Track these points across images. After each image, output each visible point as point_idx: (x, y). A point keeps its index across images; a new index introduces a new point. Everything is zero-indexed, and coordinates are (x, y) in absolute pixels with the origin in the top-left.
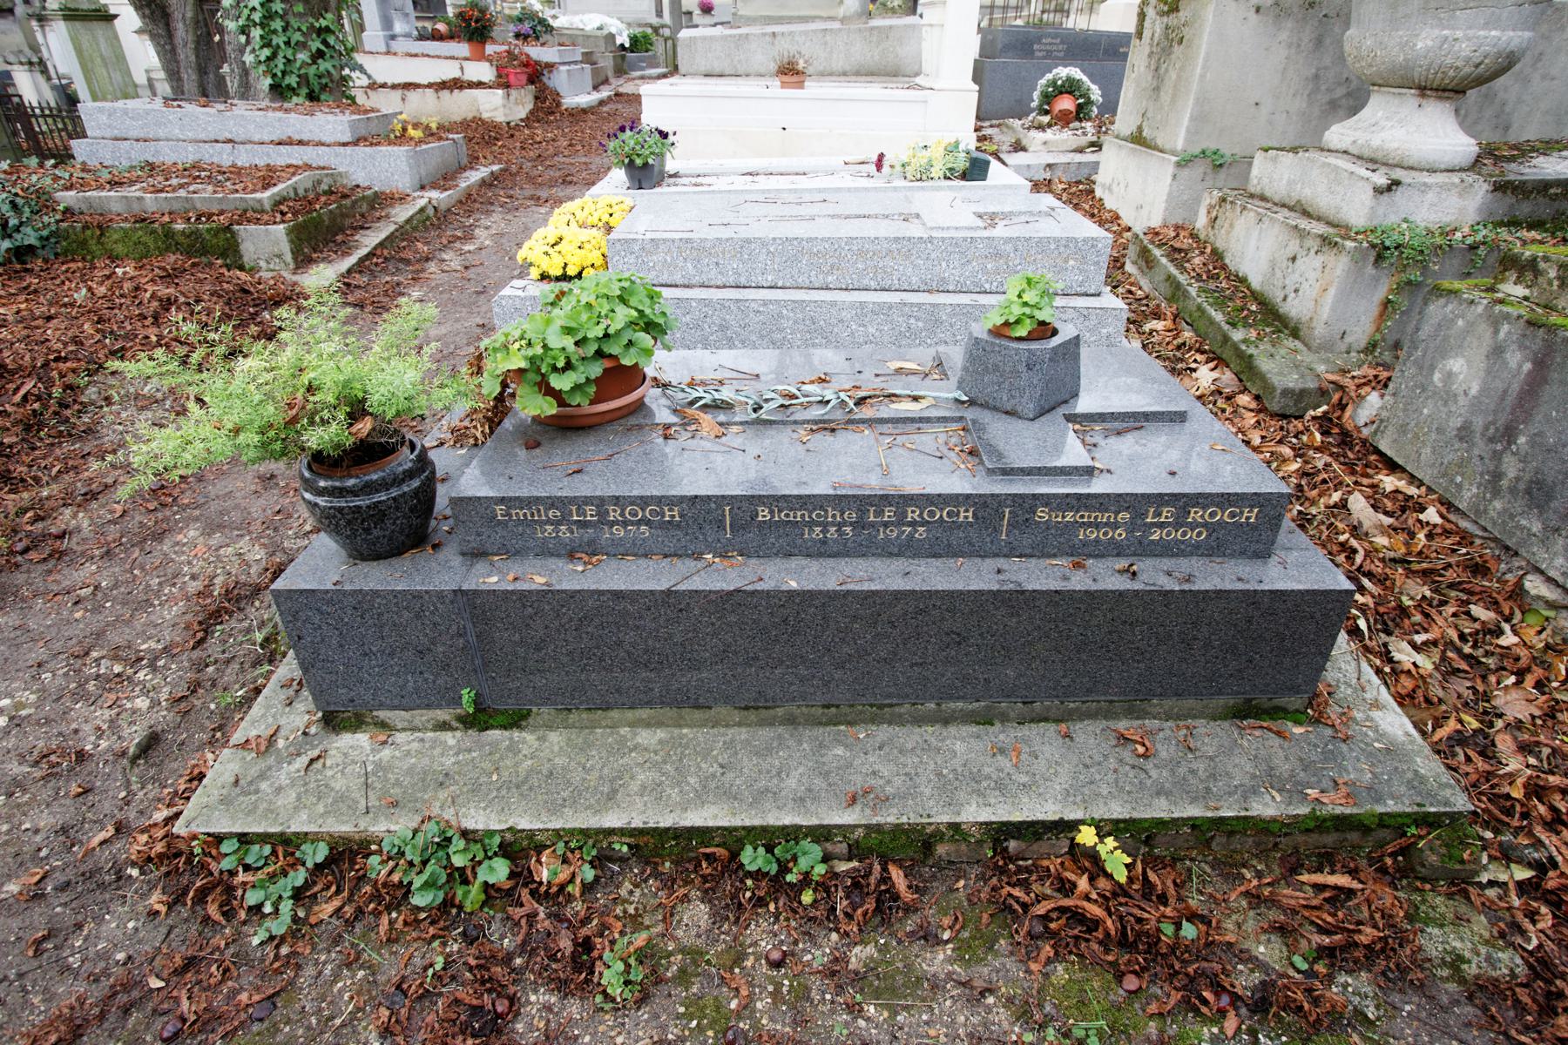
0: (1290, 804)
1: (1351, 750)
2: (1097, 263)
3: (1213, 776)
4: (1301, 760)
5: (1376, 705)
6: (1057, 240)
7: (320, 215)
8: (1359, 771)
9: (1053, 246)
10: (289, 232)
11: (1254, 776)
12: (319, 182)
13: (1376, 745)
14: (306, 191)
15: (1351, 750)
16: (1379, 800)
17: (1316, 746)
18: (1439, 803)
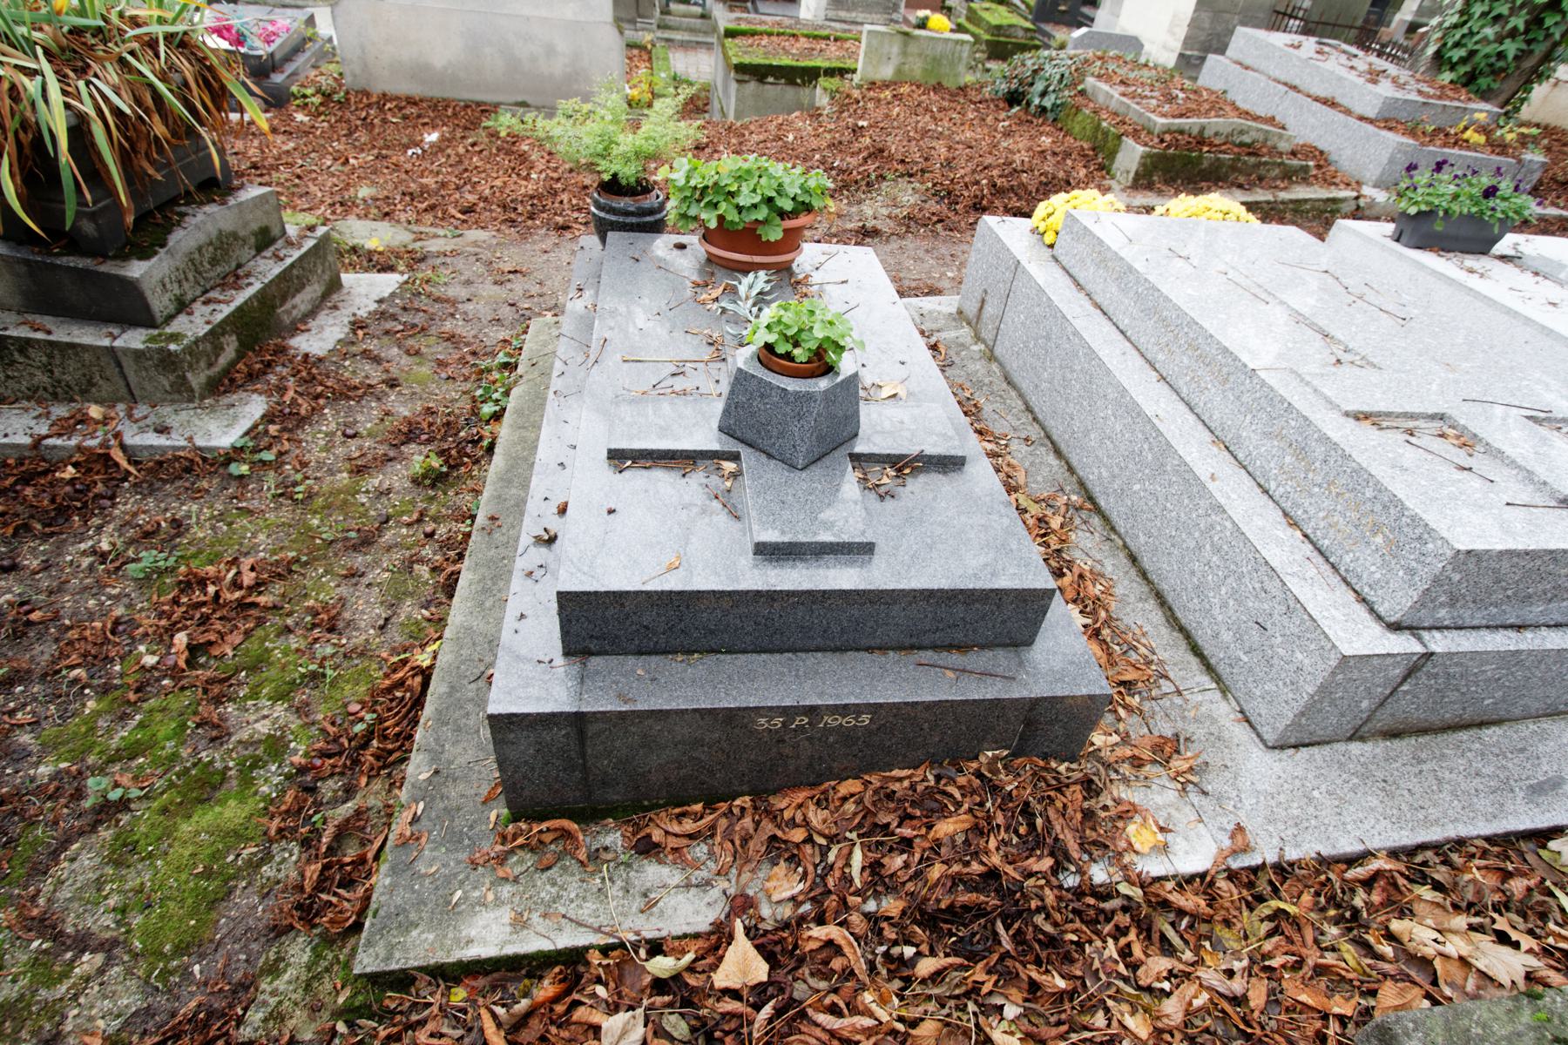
0: (413, 786)
1: (458, 862)
2: (1411, 572)
3: (458, 729)
4: (459, 809)
5: (520, 923)
6: (1380, 488)
7: (1200, 157)
8: (432, 861)
9: (1369, 493)
10: (1145, 156)
11: (450, 762)
12: (1241, 132)
13: (459, 893)
14: (1216, 134)
15: (458, 862)
16: (394, 870)
17: (471, 827)
18: (372, 934)
